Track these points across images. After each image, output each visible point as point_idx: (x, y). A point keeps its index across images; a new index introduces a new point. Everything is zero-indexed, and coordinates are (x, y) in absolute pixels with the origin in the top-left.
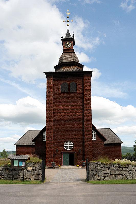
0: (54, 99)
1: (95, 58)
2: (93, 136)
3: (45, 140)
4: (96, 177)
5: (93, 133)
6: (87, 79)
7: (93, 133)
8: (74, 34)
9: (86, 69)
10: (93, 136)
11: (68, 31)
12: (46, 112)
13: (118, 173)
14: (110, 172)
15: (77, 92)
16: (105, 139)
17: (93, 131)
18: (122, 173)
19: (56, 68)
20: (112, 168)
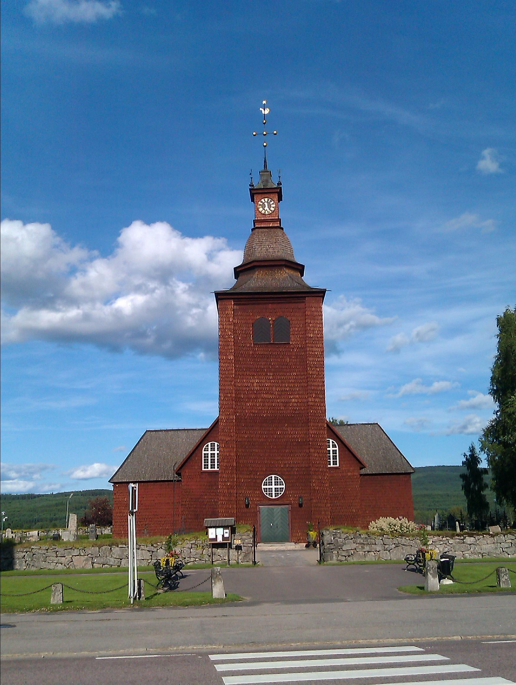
0: (237, 361)
1: (328, 449)
2: (331, 455)
3: (216, 469)
4: (334, 555)
5: (331, 446)
6: (313, 309)
7: (331, 446)
8: (280, 177)
9: (310, 279)
10: (331, 455)
11: (265, 162)
12: (220, 396)
13: (367, 548)
14: (355, 547)
15: (291, 343)
16: (363, 467)
17: (331, 441)
18: (373, 549)
19: (238, 272)
20: (359, 540)
